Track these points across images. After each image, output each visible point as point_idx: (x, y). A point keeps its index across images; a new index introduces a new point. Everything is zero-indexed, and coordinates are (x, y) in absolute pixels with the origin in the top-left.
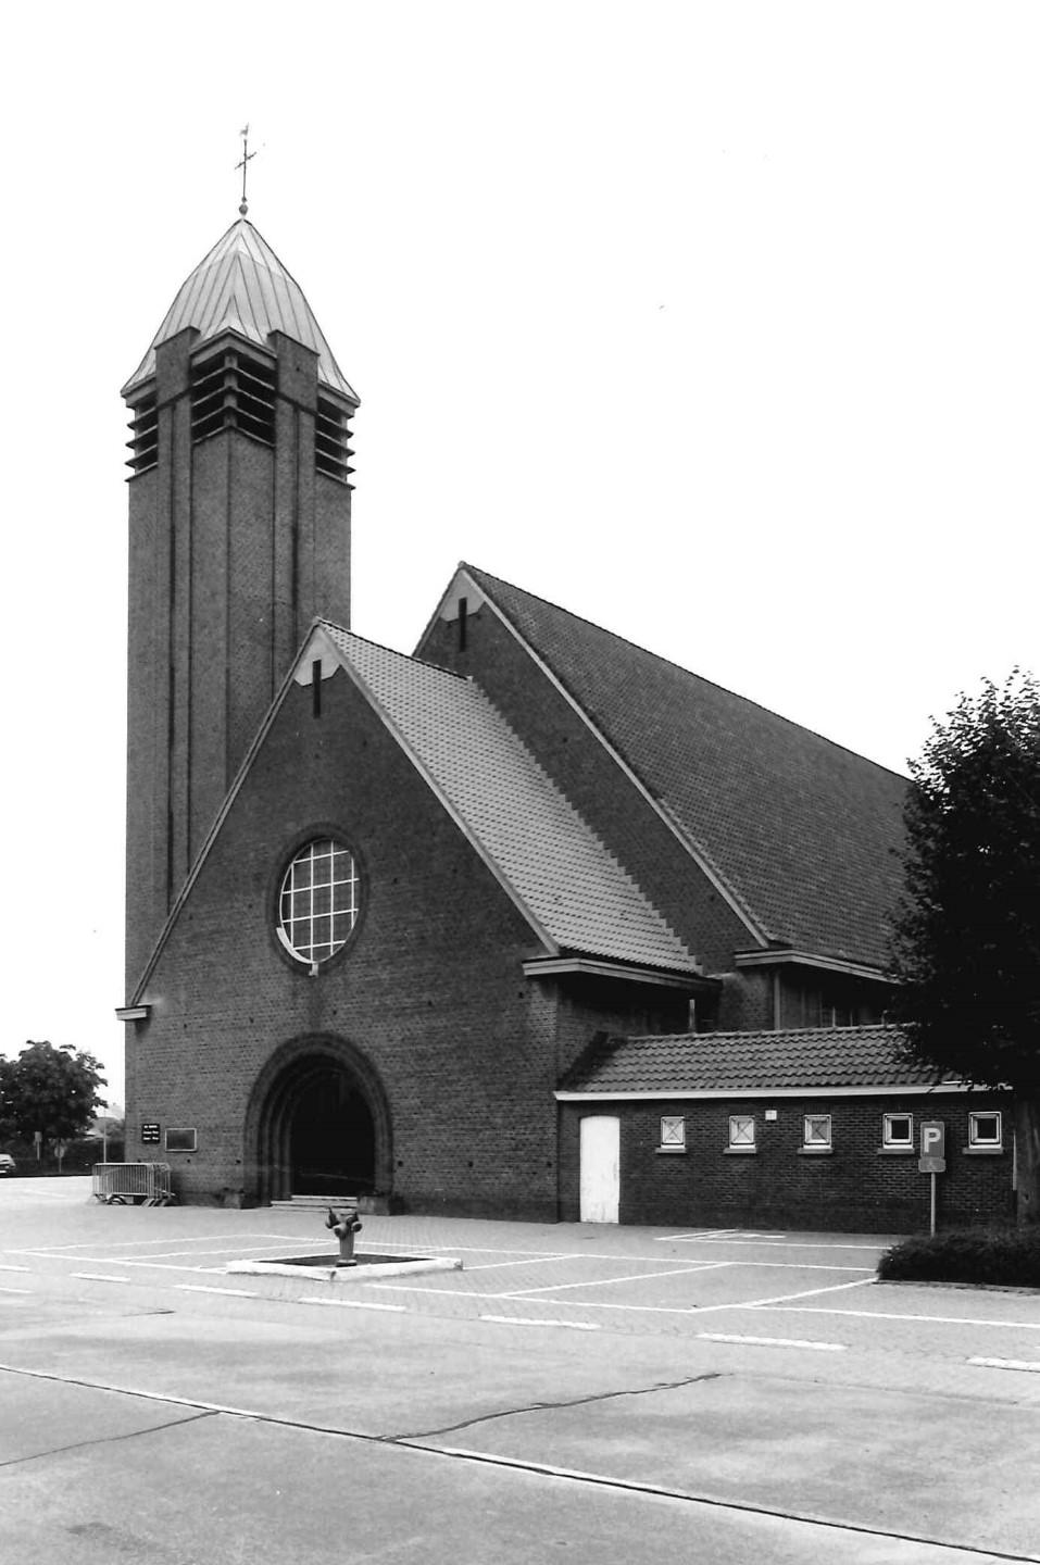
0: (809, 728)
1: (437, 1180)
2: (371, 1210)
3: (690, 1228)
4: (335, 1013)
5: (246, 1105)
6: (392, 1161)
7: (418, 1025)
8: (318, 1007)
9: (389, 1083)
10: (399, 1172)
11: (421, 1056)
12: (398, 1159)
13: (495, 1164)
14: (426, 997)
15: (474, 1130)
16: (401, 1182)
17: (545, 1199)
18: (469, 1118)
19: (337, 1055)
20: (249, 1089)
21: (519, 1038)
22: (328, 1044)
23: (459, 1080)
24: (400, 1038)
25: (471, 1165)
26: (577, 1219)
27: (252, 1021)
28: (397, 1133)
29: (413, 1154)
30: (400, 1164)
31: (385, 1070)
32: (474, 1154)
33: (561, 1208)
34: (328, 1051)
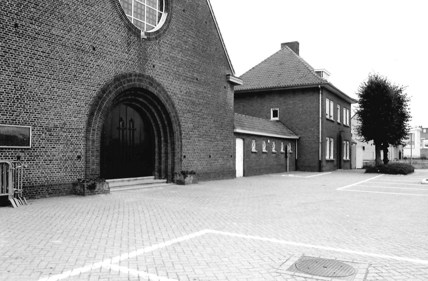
0: (275, 52)
1: (199, 164)
2: (191, 181)
3: (74, 195)
4: (154, 66)
5: (88, 112)
6: (181, 156)
7: (192, 88)
8: (143, 58)
9: (180, 114)
10: (184, 160)
11: (193, 103)
12: (183, 154)
13: (218, 156)
14: (195, 75)
15: (211, 141)
16: (185, 165)
17: (231, 170)
18: (210, 136)
19: (155, 92)
20: (91, 101)
21: (224, 105)
22: (151, 85)
23: (207, 118)
24: (185, 91)
25: (210, 157)
26: (235, 177)
27: (94, 49)
28: (183, 141)
29: (190, 152)
30: (185, 157)
31: (178, 107)
32: (212, 152)
33: (232, 174)
34: (151, 89)
